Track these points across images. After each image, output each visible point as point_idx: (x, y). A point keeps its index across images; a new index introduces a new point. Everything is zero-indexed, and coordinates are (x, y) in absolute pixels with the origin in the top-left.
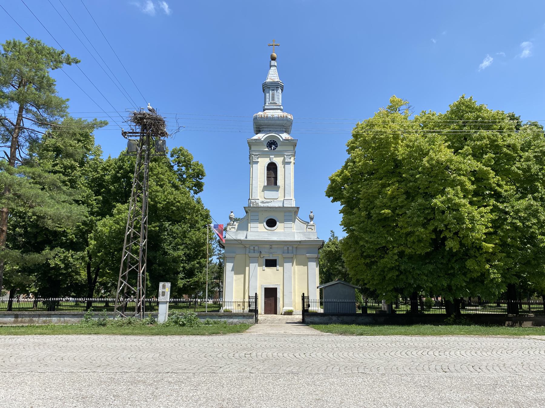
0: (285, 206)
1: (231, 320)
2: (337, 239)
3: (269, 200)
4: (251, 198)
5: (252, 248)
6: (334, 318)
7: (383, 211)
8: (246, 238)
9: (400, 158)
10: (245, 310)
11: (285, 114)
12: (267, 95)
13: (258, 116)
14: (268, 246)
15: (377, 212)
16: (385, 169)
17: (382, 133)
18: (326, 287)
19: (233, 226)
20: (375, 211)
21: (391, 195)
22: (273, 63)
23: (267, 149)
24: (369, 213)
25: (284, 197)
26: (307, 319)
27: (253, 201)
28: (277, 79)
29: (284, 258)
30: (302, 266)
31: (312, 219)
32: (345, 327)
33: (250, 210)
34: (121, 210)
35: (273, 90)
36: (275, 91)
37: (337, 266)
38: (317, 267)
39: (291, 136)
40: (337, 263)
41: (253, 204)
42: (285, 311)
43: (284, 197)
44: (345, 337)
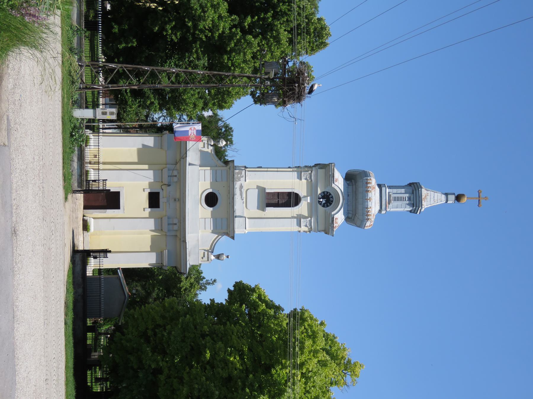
0: (236, 220)
1: (76, 159)
2: (203, 289)
3: (244, 195)
4: (247, 169)
5: (175, 173)
6: (80, 291)
7: (208, 352)
8: (190, 164)
9: (273, 371)
10: (89, 165)
11: (372, 218)
12: (403, 191)
13: (369, 178)
14: (178, 196)
15: (208, 344)
16: (262, 353)
17: (302, 349)
18: (120, 279)
19: (206, 145)
20: (209, 342)
21: (229, 360)
22: (452, 198)
23: (319, 192)
24: (207, 335)
25: (249, 218)
26: (78, 257)
27: (243, 172)
28: (426, 204)
29: (162, 218)
30: (150, 244)
31: (218, 257)
32: (71, 306)
33: (230, 169)
34: (218, 8)
35: (409, 199)
36: (408, 202)
37: (156, 290)
38: (149, 265)
39: (340, 227)
40: (162, 291)
41: (238, 173)
42: (88, 221)
43: (249, 218)
44: (63, 307)
